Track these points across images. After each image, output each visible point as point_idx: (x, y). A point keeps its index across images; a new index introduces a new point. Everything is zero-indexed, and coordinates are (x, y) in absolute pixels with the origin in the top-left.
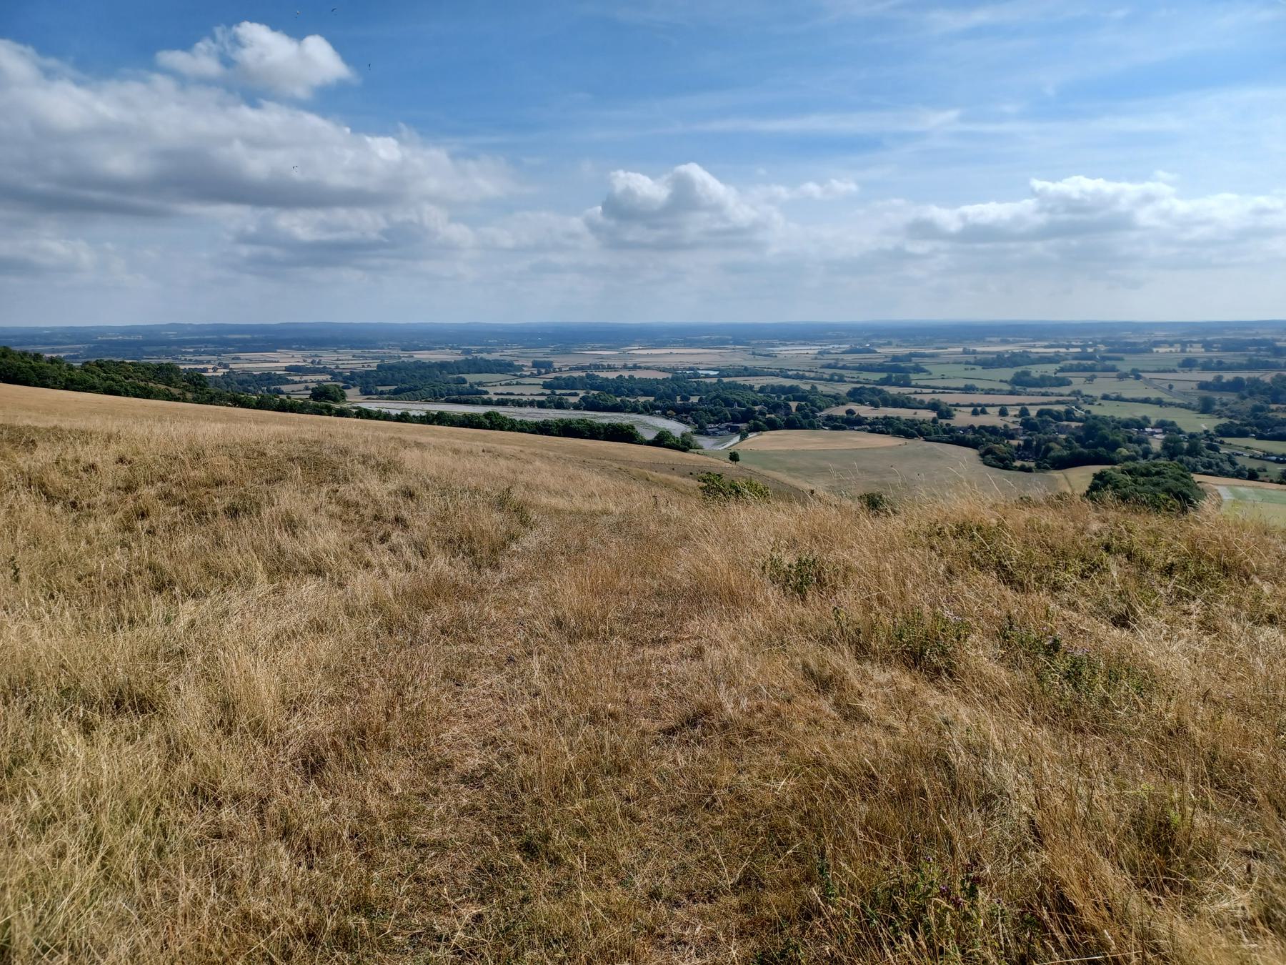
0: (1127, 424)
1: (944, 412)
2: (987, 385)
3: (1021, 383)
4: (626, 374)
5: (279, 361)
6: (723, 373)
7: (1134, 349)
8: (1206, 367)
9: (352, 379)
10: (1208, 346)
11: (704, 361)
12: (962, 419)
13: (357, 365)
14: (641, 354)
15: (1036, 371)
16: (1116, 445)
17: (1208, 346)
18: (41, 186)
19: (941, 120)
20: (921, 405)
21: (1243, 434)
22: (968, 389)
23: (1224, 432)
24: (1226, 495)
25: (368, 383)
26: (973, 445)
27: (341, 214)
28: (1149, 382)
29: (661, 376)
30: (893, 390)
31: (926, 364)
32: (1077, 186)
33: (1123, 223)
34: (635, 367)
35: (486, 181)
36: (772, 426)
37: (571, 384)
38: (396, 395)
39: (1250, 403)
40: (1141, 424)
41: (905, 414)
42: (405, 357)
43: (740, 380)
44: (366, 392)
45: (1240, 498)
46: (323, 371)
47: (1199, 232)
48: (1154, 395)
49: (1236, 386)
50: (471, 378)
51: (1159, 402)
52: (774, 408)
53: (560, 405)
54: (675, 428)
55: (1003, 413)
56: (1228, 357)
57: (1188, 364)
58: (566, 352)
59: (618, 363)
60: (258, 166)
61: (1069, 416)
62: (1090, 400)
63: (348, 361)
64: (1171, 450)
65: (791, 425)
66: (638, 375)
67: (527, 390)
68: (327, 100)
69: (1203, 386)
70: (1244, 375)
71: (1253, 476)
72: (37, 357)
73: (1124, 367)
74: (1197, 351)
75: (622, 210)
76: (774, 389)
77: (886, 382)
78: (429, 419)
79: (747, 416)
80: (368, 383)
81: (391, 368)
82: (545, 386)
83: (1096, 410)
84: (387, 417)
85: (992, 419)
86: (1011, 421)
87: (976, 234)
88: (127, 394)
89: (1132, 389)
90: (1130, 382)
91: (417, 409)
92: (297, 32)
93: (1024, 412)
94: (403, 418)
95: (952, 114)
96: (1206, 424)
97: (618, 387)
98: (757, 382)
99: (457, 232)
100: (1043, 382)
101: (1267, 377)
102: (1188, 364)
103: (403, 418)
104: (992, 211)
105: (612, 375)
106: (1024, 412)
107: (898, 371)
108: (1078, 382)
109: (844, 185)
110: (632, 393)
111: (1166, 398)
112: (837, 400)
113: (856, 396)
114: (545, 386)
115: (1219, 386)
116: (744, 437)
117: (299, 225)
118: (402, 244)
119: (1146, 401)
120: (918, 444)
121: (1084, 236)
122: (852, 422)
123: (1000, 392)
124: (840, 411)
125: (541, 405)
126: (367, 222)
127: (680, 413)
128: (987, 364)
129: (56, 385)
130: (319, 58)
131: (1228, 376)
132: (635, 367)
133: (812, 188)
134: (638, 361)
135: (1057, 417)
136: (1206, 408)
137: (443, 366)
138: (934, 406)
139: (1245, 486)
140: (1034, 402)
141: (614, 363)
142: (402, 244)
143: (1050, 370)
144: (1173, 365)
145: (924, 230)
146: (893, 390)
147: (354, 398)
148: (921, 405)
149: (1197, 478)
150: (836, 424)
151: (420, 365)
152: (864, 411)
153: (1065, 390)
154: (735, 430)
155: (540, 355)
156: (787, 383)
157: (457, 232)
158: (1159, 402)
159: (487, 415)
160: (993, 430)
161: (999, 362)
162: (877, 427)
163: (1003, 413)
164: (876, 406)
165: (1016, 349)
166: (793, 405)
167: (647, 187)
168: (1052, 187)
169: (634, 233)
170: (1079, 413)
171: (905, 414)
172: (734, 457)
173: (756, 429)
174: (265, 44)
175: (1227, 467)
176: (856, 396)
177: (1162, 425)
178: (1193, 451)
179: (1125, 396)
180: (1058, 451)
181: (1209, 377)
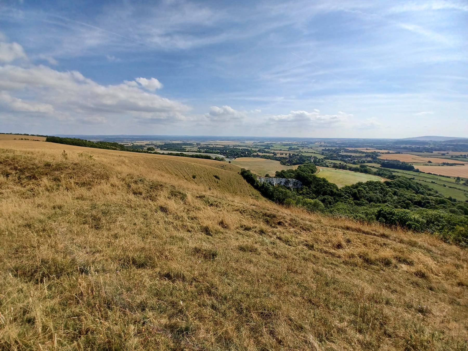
0: (308, 157)
1: (275, 154)
2: (284, 149)
3: (290, 149)
4: (215, 146)
5: (144, 143)
6: (234, 146)
7: (311, 143)
8: (324, 147)
9: (158, 147)
10: (325, 143)
11: (231, 144)
12: (278, 155)
13: (161, 144)
14: (218, 142)
15: (293, 147)
16: (305, 161)
17: (325, 143)
18: (92, 106)
19: (280, 99)
20: (271, 153)
21: (328, 159)
22: (280, 150)
23: (325, 158)
24: (321, 170)
25: (161, 147)
26: (279, 160)
27: (158, 113)
28: (313, 149)
29: (222, 146)
30: (266, 150)
31: (274, 145)
32: (298, 112)
33: (308, 119)
34: (217, 145)
35: (188, 108)
36: (242, 156)
37: (203, 148)
38: (167, 150)
39: (330, 153)
40: (310, 157)
41: (268, 154)
42: (171, 142)
43: (237, 148)
44: (161, 149)
45: (323, 170)
46: (153, 145)
47: (322, 121)
48: (314, 151)
49: (328, 150)
50: (183, 146)
51: (315, 153)
52: (243, 153)
53: (200, 152)
54: (221, 156)
55: (286, 155)
56: (328, 145)
57: (321, 146)
58: (204, 142)
59: (214, 144)
60: (141, 104)
61: (298, 155)
62: (302, 152)
63: (159, 143)
64: (315, 162)
65: (245, 156)
66: (217, 146)
67: (194, 149)
68: (158, 92)
69: (323, 150)
70: (330, 148)
71: (328, 167)
72: (86, 141)
73: (309, 146)
74: (323, 144)
75: (213, 114)
76: (244, 149)
77: (265, 148)
78: (177, 155)
79: (237, 154)
80: (161, 147)
81: (167, 144)
82: (198, 148)
83: (303, 154)
84: (160, 154)
85: (284, 156)
86: (287, 156)
87: (281, 121)
88: (104, 148)
89: (310, 150)
90: (310, 149)
91: (166, 152)
92: (148, 77)
93: (290, 154)
94: (163, 154)
95: (282, 98)
96: (322, 157)
97: (212, 149)
98: (240, 148)
99: (183, 117)
100: (294, 149)
101: (334, 148)
102: (321, 146)
103: (163, 154)
104: (284, 117)
105: (212, 146)
106: (290, 154)
107: (268, 146)
108: (301, 149)
109: (258, 110)
110: (215, 150)
111: (316, 152)
112: (255, 152)
113: (259, 151)
114: (198, 148)
115: (325, 150)
116: (235, 159)
117: (148, 115)
118: (171, 120)
119: (312, 153)
120: (269, 160)
121: (301, 121)
122: (258, 156)
123: (286, 151)
124: (256, 154)
125: (196, 152)
126: (163, 115)
127: (224, 154)
128: (284, 145)
129: (88, 146)
130: (156, 83)
131: (327, 148)
132: (217, 145)
133: (252, 111)
134: (218, 143)
135: (296, 155)
136: (323, 154)
137: (178, 144)
138: (273, 153)
139: (325, 168)
140: (292, 153)
141: (213, 144)
142: (171, 120)
143: (296, 147)
144: (318, 146)
145: (273, 120)
146: (266, 150)
147: (159, 151)
148: (271, 153)
149: (317, 167)
150: (254, 156)
151: (173, 144)
152: (260, 154)
153: (298, 150)
154: (234, 157)
155: (198, 142)
156: (246, 148)
157: (183, 117)
158: (315, 153)
159: (181, 153)
160: (284, 158)
161: (287, 145)
162: (262, 157)
163: (286, 155)
164: (263, 153)
165: (290, 143)
166: (247, 152)
167: (217, 109)
168: (294, 112)
169: (216, 118)
170: (300, 155)
171: (268, 154)
172: (230, 162)
173: (238, 157)
174: (143, 81)
175: (324, 165)
176: (259, 151)
177: (314, 157)
178: (319, 162)
179: (13, 133)
180: (294, 162)
181: (324, 148)
